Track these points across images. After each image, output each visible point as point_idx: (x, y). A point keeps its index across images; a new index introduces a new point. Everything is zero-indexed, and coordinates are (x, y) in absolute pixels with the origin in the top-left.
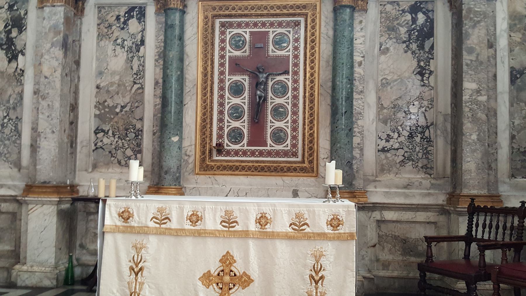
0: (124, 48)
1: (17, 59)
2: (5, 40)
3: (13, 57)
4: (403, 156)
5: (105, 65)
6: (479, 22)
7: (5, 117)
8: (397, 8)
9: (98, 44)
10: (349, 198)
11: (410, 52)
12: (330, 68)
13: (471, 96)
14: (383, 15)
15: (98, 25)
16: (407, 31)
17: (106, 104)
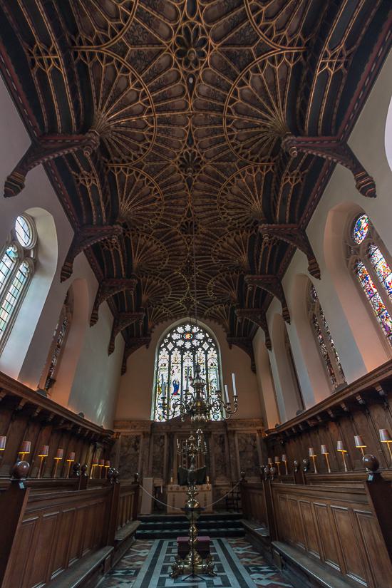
3: (136, 449)
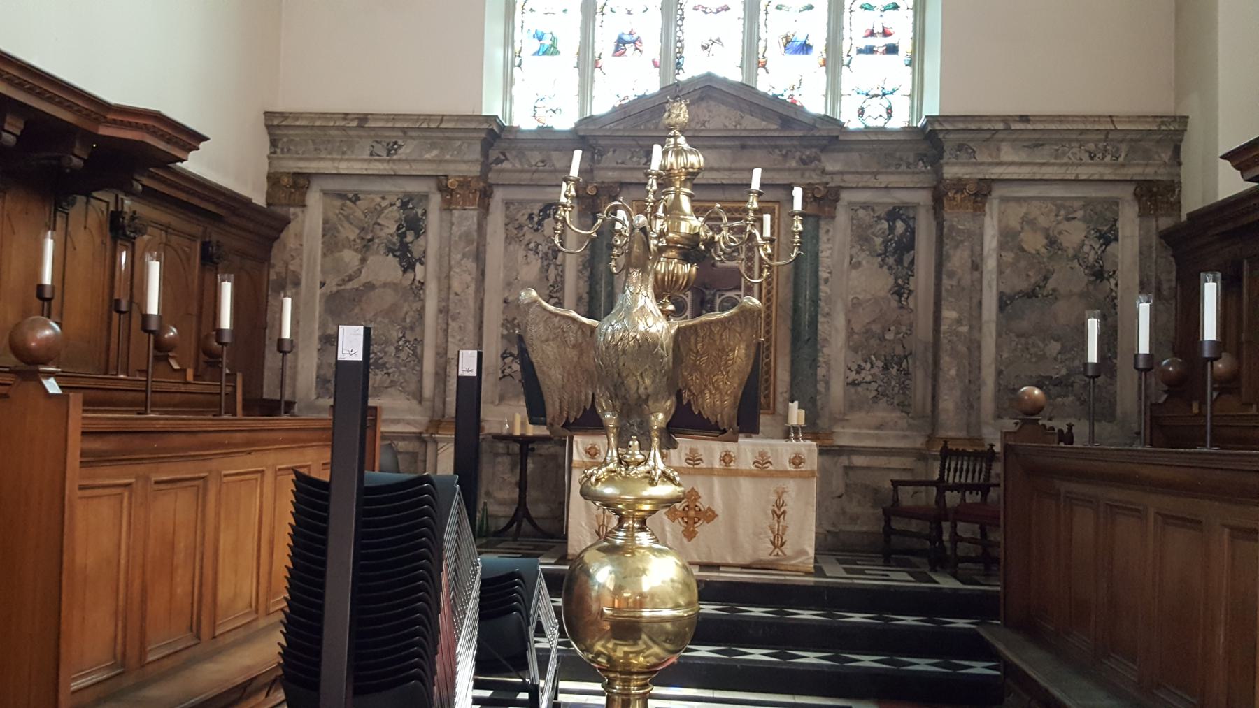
0: (538, 253)
1: (414, 269)
2: (398, 244)
3: (409, 267)
4: (877, 390)
5: (515, 274)
6: (962, 242)
7: (401, 339)
8: (872, 214)
9: (506, 248)
10: (812, 440)
11: (885, 267)
12: (791, 285)
13: (950, 326)
14: (855, 222)
15: (506, 225)
16: (883, 242)
17: (516, 322)
